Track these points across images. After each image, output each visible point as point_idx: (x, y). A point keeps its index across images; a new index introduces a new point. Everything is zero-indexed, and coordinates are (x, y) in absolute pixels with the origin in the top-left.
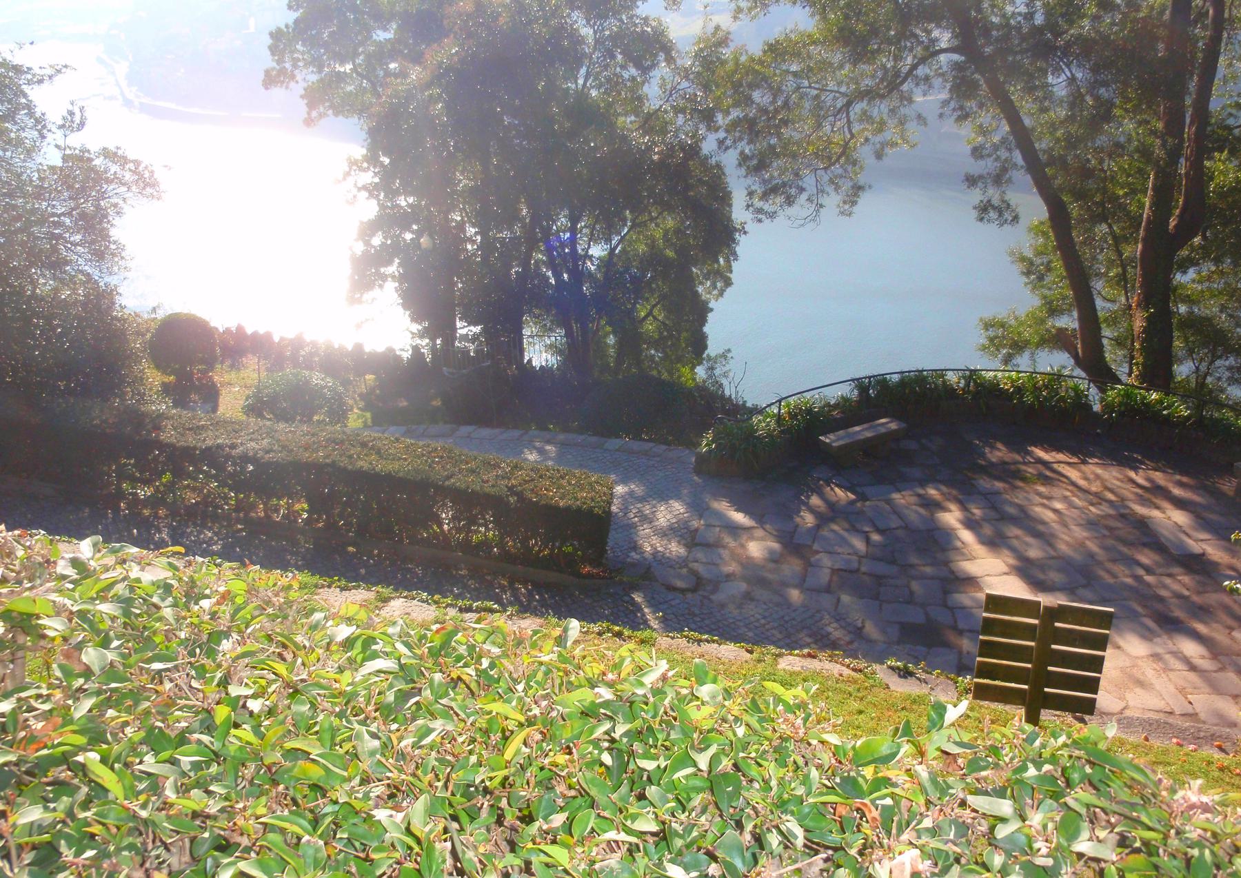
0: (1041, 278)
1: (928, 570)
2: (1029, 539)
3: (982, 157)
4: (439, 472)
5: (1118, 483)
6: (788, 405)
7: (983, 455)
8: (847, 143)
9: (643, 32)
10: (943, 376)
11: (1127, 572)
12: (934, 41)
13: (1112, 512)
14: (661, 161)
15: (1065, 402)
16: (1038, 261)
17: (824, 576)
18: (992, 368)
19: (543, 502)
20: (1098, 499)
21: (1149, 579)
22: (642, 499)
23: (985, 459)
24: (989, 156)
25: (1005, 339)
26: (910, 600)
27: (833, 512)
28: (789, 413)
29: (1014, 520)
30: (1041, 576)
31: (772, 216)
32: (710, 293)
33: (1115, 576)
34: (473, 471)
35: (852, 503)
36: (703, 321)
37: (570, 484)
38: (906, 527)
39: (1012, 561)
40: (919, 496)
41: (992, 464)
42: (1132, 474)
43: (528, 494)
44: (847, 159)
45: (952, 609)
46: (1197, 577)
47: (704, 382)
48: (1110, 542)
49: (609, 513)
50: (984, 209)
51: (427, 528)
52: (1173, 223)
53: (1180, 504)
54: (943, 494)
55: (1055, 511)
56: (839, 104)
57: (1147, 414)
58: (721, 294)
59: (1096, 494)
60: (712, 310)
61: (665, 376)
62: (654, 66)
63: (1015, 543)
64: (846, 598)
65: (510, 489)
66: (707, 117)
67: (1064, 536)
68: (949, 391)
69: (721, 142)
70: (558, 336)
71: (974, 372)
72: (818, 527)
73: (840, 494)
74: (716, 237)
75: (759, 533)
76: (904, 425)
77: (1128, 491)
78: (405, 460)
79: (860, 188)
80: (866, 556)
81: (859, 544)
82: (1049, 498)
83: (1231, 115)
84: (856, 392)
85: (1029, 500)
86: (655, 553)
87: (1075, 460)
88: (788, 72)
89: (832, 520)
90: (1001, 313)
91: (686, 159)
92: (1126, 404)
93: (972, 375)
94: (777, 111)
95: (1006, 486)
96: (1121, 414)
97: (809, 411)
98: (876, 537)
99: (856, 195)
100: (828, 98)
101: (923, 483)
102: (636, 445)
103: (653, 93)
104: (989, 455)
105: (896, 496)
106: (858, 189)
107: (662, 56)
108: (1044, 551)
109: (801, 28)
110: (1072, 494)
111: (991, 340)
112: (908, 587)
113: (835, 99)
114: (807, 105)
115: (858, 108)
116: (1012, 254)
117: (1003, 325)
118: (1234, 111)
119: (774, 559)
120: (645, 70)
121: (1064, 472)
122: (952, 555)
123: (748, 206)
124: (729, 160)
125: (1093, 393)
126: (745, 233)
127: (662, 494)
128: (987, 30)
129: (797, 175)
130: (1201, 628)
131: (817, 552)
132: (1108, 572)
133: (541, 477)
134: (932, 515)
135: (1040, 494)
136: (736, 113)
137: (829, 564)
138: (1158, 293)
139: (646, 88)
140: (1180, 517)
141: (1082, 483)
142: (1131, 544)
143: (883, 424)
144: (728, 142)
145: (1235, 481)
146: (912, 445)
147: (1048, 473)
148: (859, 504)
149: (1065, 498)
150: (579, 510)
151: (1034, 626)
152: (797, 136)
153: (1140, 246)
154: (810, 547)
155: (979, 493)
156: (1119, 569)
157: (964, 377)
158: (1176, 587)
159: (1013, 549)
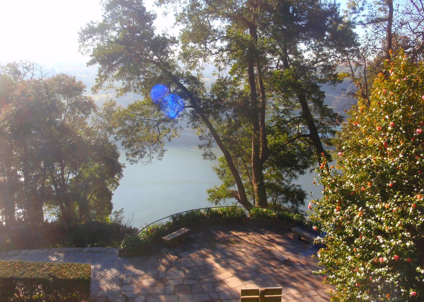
0: (223, 175)
1: (207, 280)
2: (237, 263)
3: (202, 139)
4: (17, 274)
5: (260, 240)
6: (150, 227)
7: (216, 236)
8: (159, 137)
9: (85, 101)
10: (200, 211)
11: (269, 269)
12: (184, 104)
13: (260, 250)
14: (95, 145)
15: (239, 215)
16: (221, 170)
17: (172, 288)
18: (214, 207)
19: (64, 278)
20: (255, 246)
21: (276, 270)
22: (101, 270)
23: (218, 237)
24: (205, 139)
25: (216, 196)
26: (203, 292)
27: (171, 264)
28: (150, 230)
29: (231, 257)
30: (243, 275)
31: (136, 162)
32: (111, 188)
33: (265, 271)
34: (33, 270)
35: (177, 260)
36: (110, 198)
37: (74, 269)
38: (197, 266)
39: (233, 272)
40: (199, 254)
41: (220, 239)
42: (263, 236)
43: (57, 276)
44: (159, 142)
45: (217, 293)
46: (289, 267)
47: (115, 220)
48: (262, 260)
49: (90, 278)
50: (205, 155)
51: (12, 296)
52: (260, 156)
53: (279, 244)
54: (206, 252)
55: (243, 252)
56: (155, 124)
57: (264, 216)
58: (116, 188)
59: (254, 244)
60: (113, 194)
61: (99, 220)
62: (90, 113)
63: (233, 265)
64: (181, 295)
65: (50, 275)
66: (110, 130)
67: (247, 260)
68: (202, 216)
69: (115, 138)
70: (56, 209)
71: (209, 209)
72: (167, 270)
73: (173, 257)
74: (114, 169)
75: (146, 276)
76: (190, 230)
77: (263, 242)
78: (3, 269)
79: (164, 151)
80: (185, 279)
81: (182, 274)
82: (240, 248)
83: (270, 123)
84: (172, 220)
85: (234, 249)
86: (108, 290)
87: (245, 234)
88: (137, 114)
89: (171, 267)
90: (213, 188)
91: (103, 144)
92: (257, 214)
93: (209, 210)
94: (134, 127)
95: (226, 246)
96: (256, 217)
97: (157, 229)
98: (187, 271)
99: (163, 153)
100: (151, 123)
101: (199, 249)
102: (95, 249)
103: (89, 122)
104: (218, 236)
105: (191, 255)
106: (163, 151)
107: (92, 109)
108: (243, 266)
109: (140, 100)
110: (247, 245)
111: (211, 196)
112: (201, 287)
113: (153, 123)
114: (144, 124)
115: (161, 125)
116: (213, 168)
117: (214, 191)
118: (271, 122)
119: (153, 286)
120: (87, 115)
121: (243, 238)
122: (214, 273)
123: (127, 159)
124: (119, 144)
125: (247, 212)
126: (125, 167)
127: (107, 266)
128: (199, 100)
129: (143, 148)
130: (294, 284)
131: (168, 280)
132: (263, 270)
133: (62, 268)
134: (204, 260)
135: (237, 247)
136: (120, 128)
137: (173, 284)
138: (260, 178)
139: (87, 120)
140: (280, 248)
141: (249, 241)
142: (268, 260)
143: (183, 230)
144: (118, 138)
145: (292, 234)
146: (193, 236)
147: (238, 239)
148: (179, 260)
149: (245, 248)
150: (79, 278)
151: (258, 298)
152: (141, 135)
153: (252, 164)
154: (165, 278)
155: (218, 250)
156: (266, 268)
157: (206, 211)
158: (284, 271)
159: (233, 268)
